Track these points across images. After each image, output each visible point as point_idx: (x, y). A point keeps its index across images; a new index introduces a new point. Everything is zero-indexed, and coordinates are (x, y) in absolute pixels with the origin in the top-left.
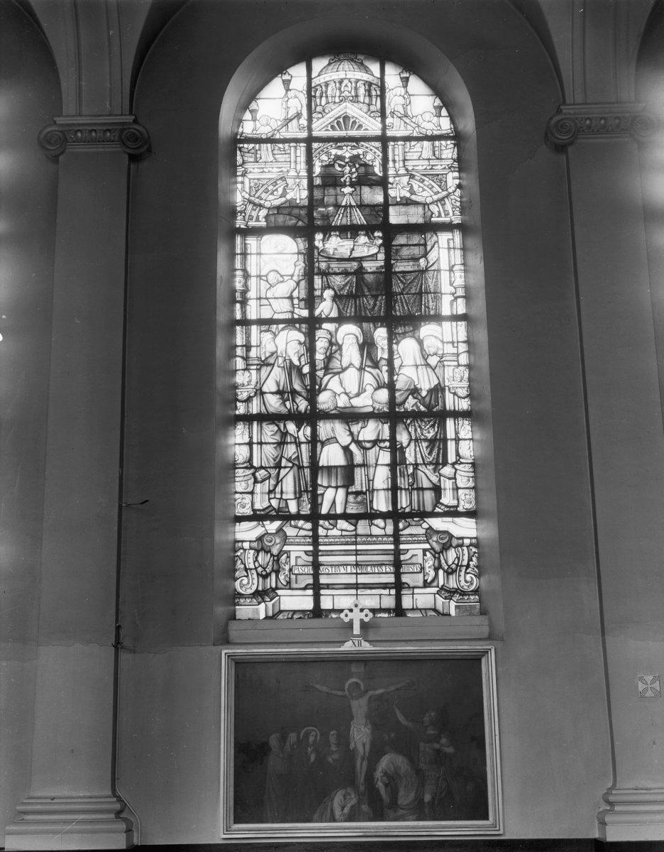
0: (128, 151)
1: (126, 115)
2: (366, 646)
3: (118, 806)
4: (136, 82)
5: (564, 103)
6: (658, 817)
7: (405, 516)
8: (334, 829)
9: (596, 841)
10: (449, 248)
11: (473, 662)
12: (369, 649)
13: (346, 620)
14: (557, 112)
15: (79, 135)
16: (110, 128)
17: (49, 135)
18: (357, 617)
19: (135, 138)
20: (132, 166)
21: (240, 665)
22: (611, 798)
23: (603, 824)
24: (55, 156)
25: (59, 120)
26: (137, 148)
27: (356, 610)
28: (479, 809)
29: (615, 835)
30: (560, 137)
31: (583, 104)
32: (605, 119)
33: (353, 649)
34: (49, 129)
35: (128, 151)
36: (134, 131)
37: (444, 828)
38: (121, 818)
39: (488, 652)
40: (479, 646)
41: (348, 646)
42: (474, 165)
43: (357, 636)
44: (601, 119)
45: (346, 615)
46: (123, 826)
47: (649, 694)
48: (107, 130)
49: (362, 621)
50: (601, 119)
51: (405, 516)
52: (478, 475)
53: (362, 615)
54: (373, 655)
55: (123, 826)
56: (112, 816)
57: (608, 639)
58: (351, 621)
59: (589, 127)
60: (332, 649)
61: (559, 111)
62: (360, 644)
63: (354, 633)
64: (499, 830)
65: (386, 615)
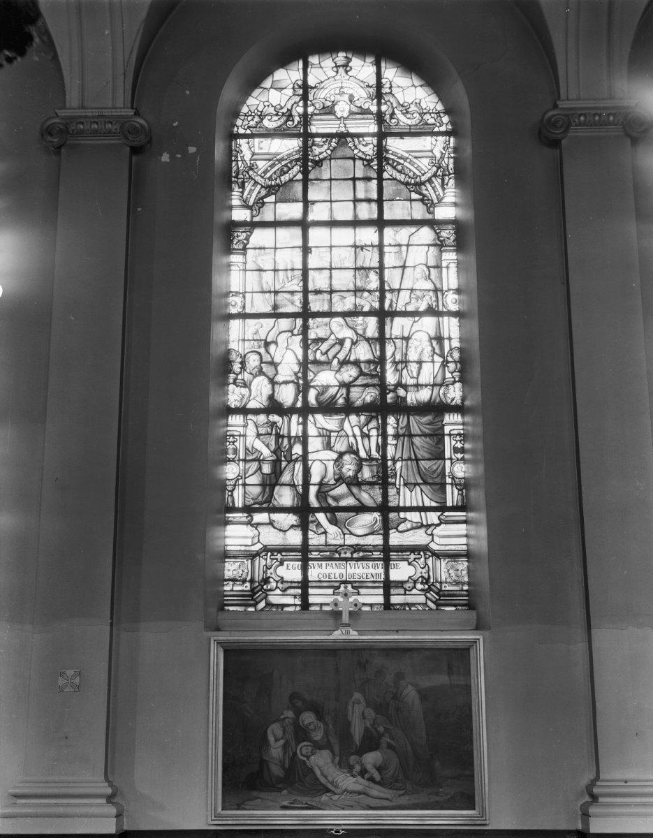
1: (127, 108)
2: (353, 635)
3: (109, 791)
4: (139, 71)
5: (559, 98)
6: (649, 810)
8: (401, 817)
9: (578, 832)
12: (357, 638)
15: (582, 118)
17: (553, 119)
19: (135, 131)
20: (134, 158)
21: (233, 654)
23: (586, 816)
24: (58, 148)
25: (62, 113)
28: (467, 800)
29: (597, 827)
30: (552, 131)
31: (577, 100)
32: (585, 115)
34: (551, 113)
36: (138, 125)
37: (236, 817)
38: (113, 803)
39: (476, 642)
41: (338, 635)
44: (594, 115)
46: (113, 810)
47: (61, 682)
54: (353, 644)
55: (113, 810)
56: (104, 801)
57: (593, 632)
60: (384, 637)
61: (555, 106)
62: (348, 633)
64: (486, 820)
65: (453, 608)
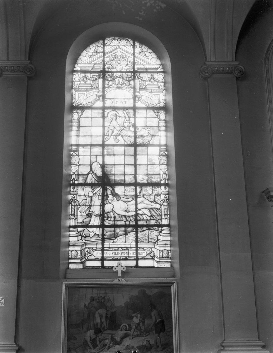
0: (27, 75)
1: (27, 60)
5: (206, 61)
7: (142, 185)
10: (159, 127)
11: (168, 286)
13: (115, 270)
14: (204, 64)
16: (217, 66)
18: (120, 269)
22: (223, 344)
26: (30, 74)
27: (119, 266)
33: (118, 282)
35: (27, 75)
39: (174, 284)
40: (170, 280)
41: (116, 281)
42: (171, 90)
43: (120, 277)
45: (115, 269)
48: (228, 67)
49: (122, 271)
50: (215, 67)
51: (142, 185)
52: (172, 233)
53: (122, 269)
58: (117, 271)
59: (217, 70)
61: (205, 64)
63: (119, 276)
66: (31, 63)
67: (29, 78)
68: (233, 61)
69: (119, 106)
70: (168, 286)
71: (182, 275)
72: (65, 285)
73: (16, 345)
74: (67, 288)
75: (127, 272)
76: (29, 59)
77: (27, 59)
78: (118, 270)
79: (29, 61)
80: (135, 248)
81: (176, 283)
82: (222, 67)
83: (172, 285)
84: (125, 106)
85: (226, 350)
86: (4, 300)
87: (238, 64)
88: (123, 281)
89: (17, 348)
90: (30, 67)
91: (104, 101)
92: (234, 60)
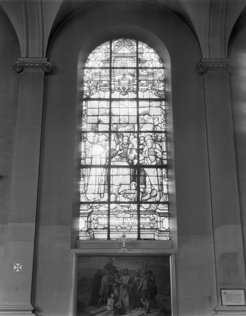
1: (44, 58)
11: (166, 257)
22: (216, 309)
39: (172, 254)
41: (121, 251)
52: (170, 209)
63: (123, 246)
66: (48, 60)
67: (46, 74)
68: (226, 59)
69: (107, 98)
70: (166, 257)
71: (179, 246)
72: (76, 254)
73: (32, 306)
74: (78, 257)
75: (131, 243)
76: (46, 57)
77: (45, 56)
78: (122, 241)
79: (47, 59)
80: (111, 233)
81: (174, 253)
82: (222, 64)
83: (170, 255)
84: (120, 98)
85: (219, 315)
86: (21, 266)
87: (230, 61)
88: (127, 251)
89: (33, 308)
90: (48, 65)
91: (137, 93)
92: (227, 58)
